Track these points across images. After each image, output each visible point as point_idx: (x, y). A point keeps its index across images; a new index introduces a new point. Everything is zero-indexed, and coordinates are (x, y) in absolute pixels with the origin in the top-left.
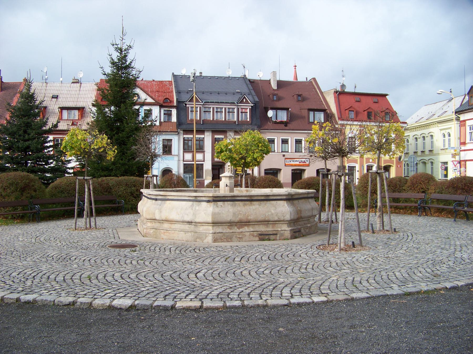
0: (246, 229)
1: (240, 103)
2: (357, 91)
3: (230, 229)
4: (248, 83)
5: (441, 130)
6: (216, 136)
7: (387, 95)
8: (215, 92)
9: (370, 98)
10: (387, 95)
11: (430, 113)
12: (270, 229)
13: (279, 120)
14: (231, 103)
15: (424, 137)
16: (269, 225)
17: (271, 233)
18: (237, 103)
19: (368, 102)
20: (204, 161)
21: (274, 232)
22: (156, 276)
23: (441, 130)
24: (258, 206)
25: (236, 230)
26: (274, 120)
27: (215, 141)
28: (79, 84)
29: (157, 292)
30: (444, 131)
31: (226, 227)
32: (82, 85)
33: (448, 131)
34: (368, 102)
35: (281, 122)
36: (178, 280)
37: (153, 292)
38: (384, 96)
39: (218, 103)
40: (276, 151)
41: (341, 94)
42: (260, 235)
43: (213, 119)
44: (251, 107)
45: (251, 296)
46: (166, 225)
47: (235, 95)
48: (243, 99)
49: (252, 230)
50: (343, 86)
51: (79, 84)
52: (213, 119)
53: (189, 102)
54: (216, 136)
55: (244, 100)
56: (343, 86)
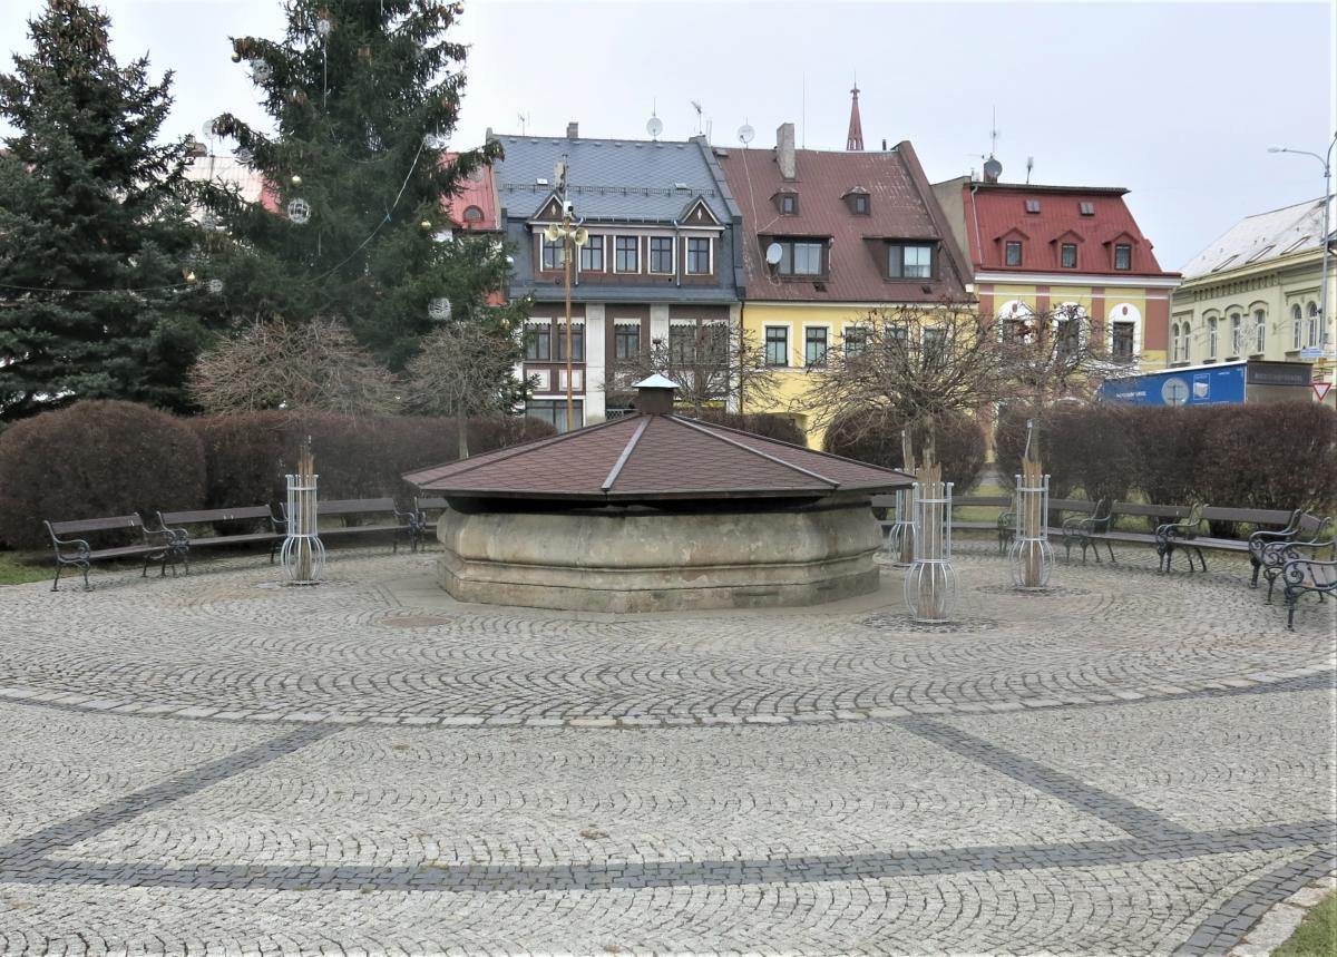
0: (703, 580)
1: (686, 224)
2: (1039, 179)
3: (668, 581)
4: (711, 159)
5: (1289, 295)
6: (618, 321)
7: (1124, 191)
8: (613, 190)
9: (1069, 203)
10: (1124, 191)
11: (1260, 241)
12: (760, 579)
13: (800, 269)
14: (662, 222)
15: (1236, 317)
16: (758, 572)
17: (762, 590)
18: (679, 223)
19: (1063, 217)
20: (583, 392)
21: (770, 588)
22: (516, 678)
23: (1289, 295)
24: (732, 527)
25: (679, 582)
26: (785, 270)
27: (614, 335)
28: (208, 159)
29: (527, 706)
30: (1297, 300)
31: (657, 576)
32: (217, 161)
33: (1308, 298)
34: (1063, 217)
35: (802, 279)
36: (564, 685)
37: (517, 705)
38: (1116, 194)
39: (623, 221)
40: (791, 364)
41: (987, 189)
42: (738, 594)
43: (610, 269)
44: (717, 236)
45: (715, 710)
46: (514, 575)
47: (672, 199)
48: (696, 211)
49: (718, 583)
50: (993, 166)
51: (208, 159)
52: (610, 269)
53: (538, 219)
54: (618, 321)
55: (700, 214)
56: (993, 166)
